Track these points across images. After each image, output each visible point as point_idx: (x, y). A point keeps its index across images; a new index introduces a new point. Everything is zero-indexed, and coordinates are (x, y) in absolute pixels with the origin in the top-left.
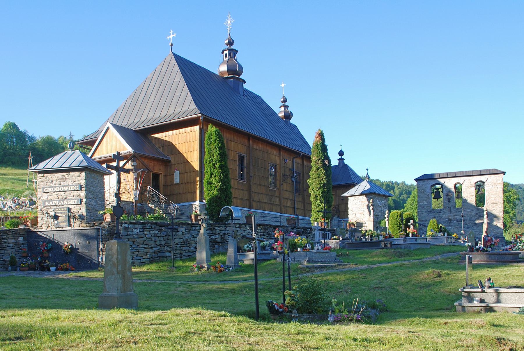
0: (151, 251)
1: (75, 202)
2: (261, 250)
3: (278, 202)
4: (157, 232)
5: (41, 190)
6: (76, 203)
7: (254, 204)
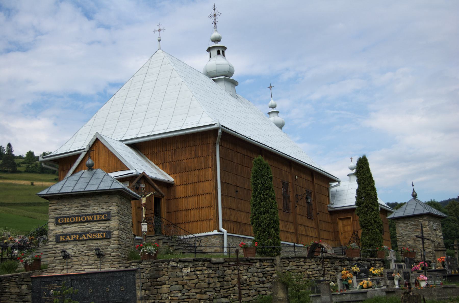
0: (205, 296)
1: (103, 235)
3: (292, 230)
4: (211, 271)
5: (53, 220)
6: (104, 236)
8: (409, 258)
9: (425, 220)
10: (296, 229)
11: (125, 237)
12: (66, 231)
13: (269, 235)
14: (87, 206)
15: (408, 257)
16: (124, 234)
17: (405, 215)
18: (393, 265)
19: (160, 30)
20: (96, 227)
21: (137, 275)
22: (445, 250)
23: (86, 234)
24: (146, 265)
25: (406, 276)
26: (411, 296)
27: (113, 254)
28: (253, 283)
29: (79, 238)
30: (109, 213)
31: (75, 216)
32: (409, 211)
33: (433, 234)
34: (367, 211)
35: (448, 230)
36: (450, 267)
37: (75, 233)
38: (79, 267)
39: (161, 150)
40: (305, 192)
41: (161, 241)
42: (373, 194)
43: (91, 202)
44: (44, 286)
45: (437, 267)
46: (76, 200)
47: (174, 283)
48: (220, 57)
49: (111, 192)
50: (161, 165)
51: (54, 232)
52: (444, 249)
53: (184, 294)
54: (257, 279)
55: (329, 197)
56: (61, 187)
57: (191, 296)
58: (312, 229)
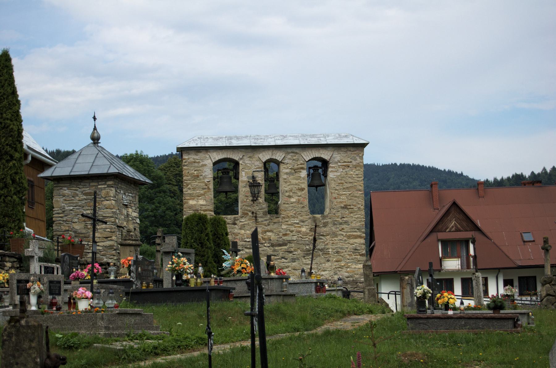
8: (70, 256)
9: (109, 186)
15: (69, 255)
17: (72, 174)
18: (35, 267)
22: (139, 245)
25: (54, 288)
26: (22, 326)
32: (82, 168)
33: (121, 213)
35: (161, 210)
36: (139, 277)
42: (15, 128)
45: (122, 274)
52: (137, 243)
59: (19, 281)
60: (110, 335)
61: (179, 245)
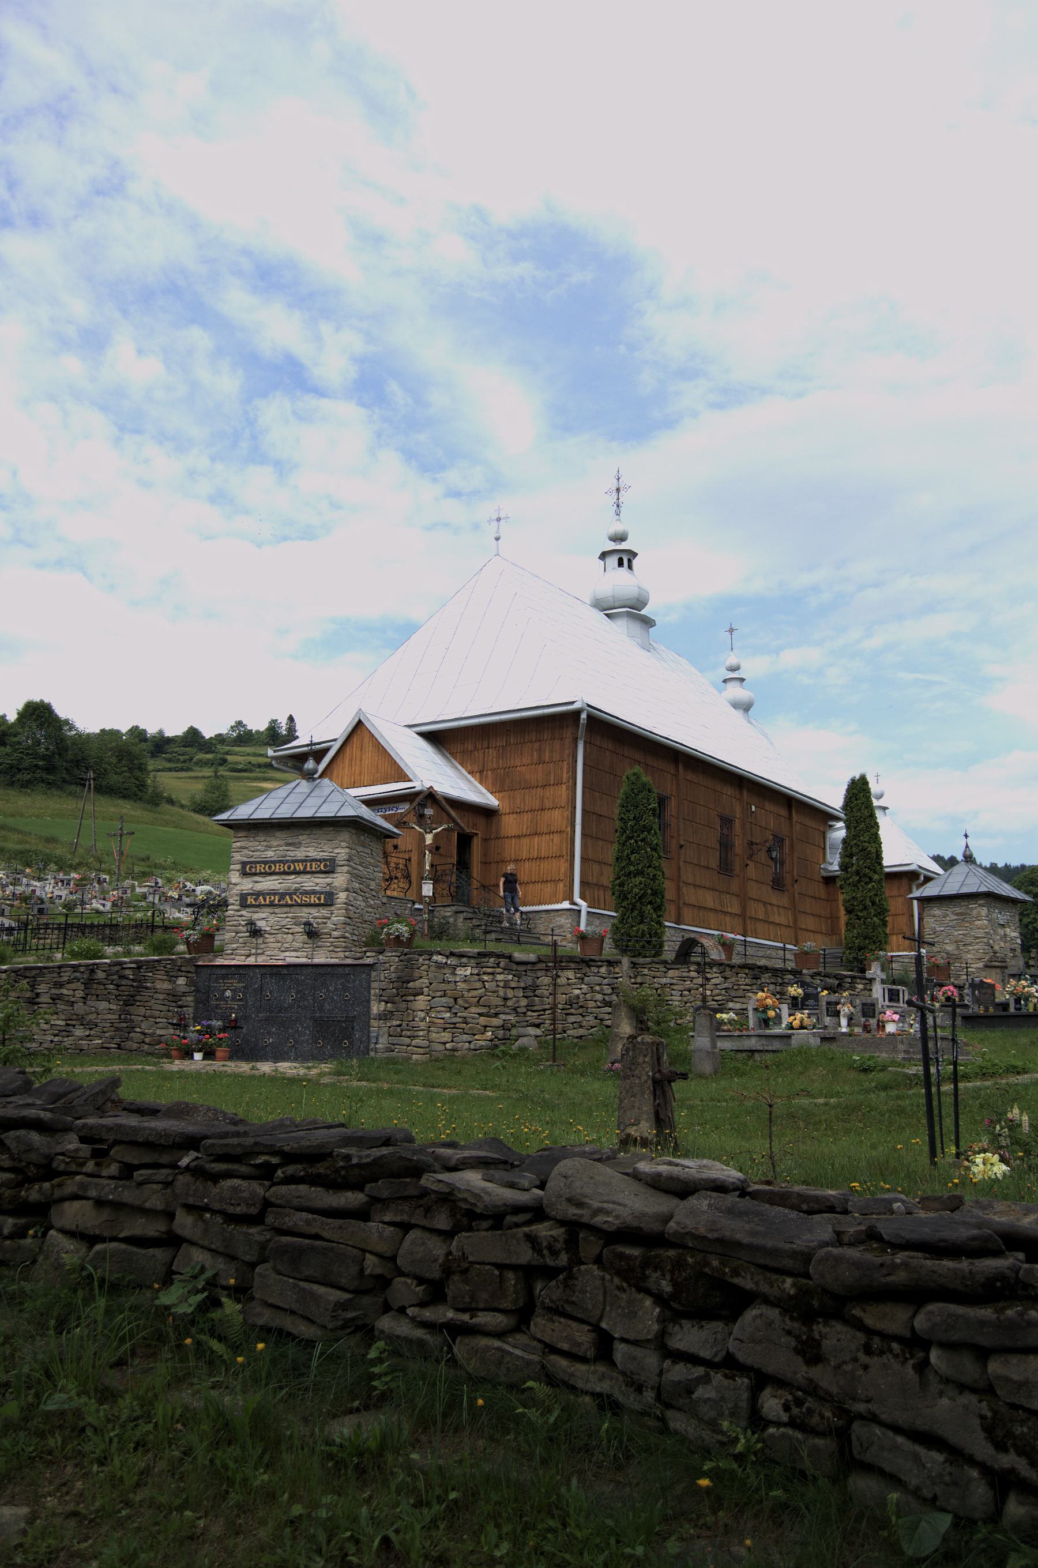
0: (496, 1022)
1: (319, 899)
2: (760, 1027)
3: (735, 909)
5: (239, 867)
6: (322, 901)
7: (687, 913)
9: (981, 905)
10: (744, 908)
11: (363, 904)
12: (259, 887)
13: (642, 917)
14: (297, 845)
16: (361, 898)
19: (499, 520)
20: (309, 883)
21: (374, 974)
23: (290, 895)
24: (391, 958)
27: (335, 934)
28: (591, 1004)
29: (279, 901)
30: (333, 860)
31: (274, 862)
34: (859, 881)
37: (273, 893)
38: (276, 952)
39: (479, 746)
40: (771, 837)
41: (462, 916)
42: (873, 850)
43: (303, 838)
44: (216, 981)
46: (278, 834)
47: (439, 994)
48: (624, 570)
49: (339, 821)
50: (478, 774)
51: (238, 887)
53: (456, 1013)
54: (599, 997)
55: (824, 849)
56: (254, 808)
57: (470, 1020)
58: (782, 910)
59: (828, 1003)
60: (909, 1060)
61: (1028, 966)
